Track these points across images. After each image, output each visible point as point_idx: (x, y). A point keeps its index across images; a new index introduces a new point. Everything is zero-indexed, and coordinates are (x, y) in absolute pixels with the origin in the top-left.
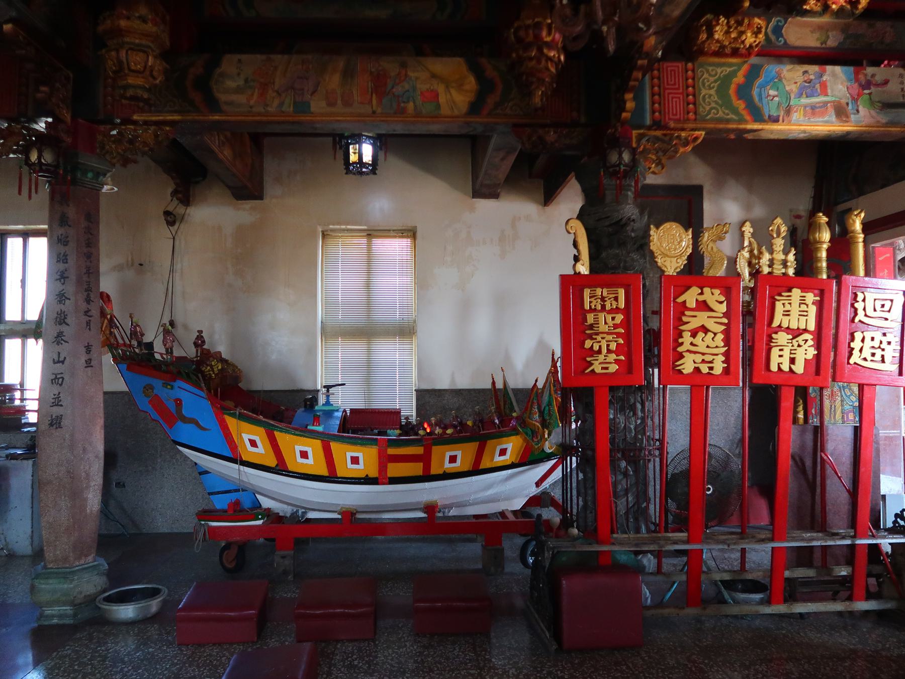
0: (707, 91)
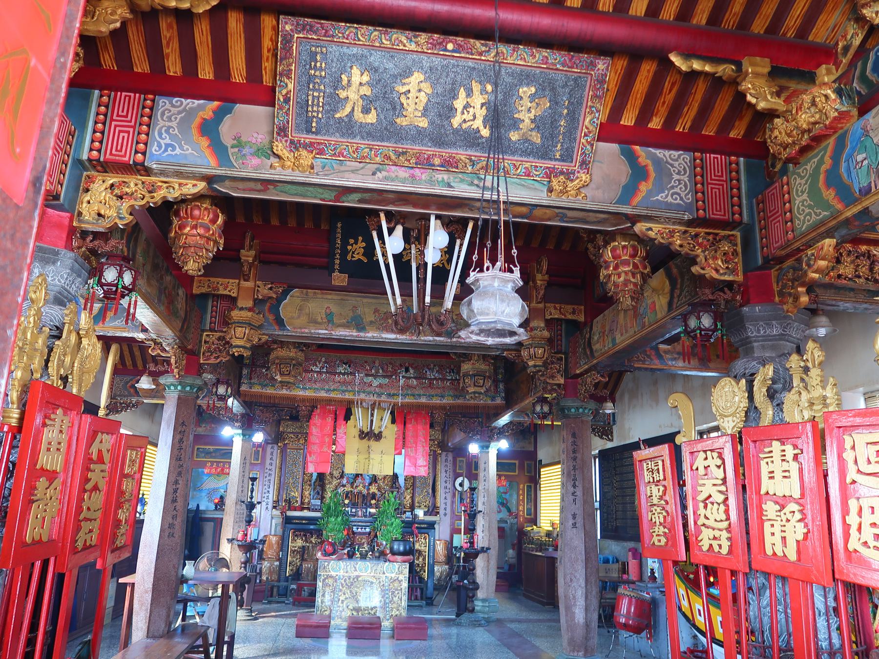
0: (682, 177)
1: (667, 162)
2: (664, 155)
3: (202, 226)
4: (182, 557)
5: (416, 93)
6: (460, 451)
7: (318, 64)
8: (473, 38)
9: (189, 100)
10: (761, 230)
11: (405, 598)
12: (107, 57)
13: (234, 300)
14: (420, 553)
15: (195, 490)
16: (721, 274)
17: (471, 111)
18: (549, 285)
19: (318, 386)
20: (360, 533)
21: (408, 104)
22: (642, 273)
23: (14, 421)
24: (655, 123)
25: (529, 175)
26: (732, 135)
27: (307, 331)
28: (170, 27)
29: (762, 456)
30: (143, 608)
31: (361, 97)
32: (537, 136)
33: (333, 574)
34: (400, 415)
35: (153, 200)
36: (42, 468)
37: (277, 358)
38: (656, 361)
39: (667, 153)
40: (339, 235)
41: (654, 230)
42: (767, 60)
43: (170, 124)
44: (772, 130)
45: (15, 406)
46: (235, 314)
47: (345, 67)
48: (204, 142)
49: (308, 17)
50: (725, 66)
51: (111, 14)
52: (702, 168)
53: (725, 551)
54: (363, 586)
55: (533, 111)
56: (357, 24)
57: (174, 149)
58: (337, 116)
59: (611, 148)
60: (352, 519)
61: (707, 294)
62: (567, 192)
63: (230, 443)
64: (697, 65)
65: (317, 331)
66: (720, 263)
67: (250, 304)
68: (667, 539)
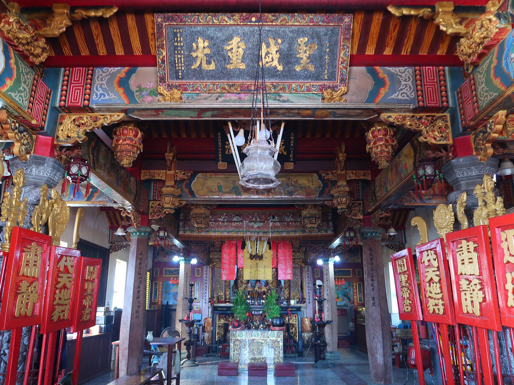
0: (407, 83)
1: (397, 74)
2: (395, 70)
3: (129, 139)
4: (145, 329)
5: (236, 49)
6: (314, 265)
7: (179, 39)
8: (267, 13)
9: (112, 68)
10: (460, 110)
11: (282, 352)
12: (66, 49)
13: (164, 181)
14: (293, 325)
15: (166, 293)
16: (438, 141)
17: (271, 56)
18: (347, 159)
19: (223, 229)
20: (256, 315)
21: (232, 56)
22: (392, 145)
23: (7, 249)
24: (388, 52)
25: (309, 91)
26: (439, 53)
27: (207, 197)
28: (96, 28)
29: (457, 250)
30: (124, 358)
31: (205, 55)
32: (312, 67)
33: (239, 338)
34: (273, 244)
35: (96, 126)
36: (23, 275)
37: (194, 214)
38: (418, 201)
39: (397, 69)
40: (220, 140)
41: (393, 117)
42: (451, 3)
43: (102, 82)
44: (460, 46)
45: (8, 242)
46: (164, 190)
47: (194, 39)
48: (121, 91)
49: (170, 12)
50: (424, 10)
51: (60, 24)
52: (420, 76)
53: (441, 312)
54: (258, 345)
55: (308, 52)
56: (198, 13)
57: (105, 96)
58: (193, 67)
59: (359, 70)
60: (252, 306)
61: (431, 154)
62: (333, 98)
63: (178, 266)
64: (405, 12)
65: (213, 197)
66: (436, 133)
67: (173, 183)
68: (411, 307)
